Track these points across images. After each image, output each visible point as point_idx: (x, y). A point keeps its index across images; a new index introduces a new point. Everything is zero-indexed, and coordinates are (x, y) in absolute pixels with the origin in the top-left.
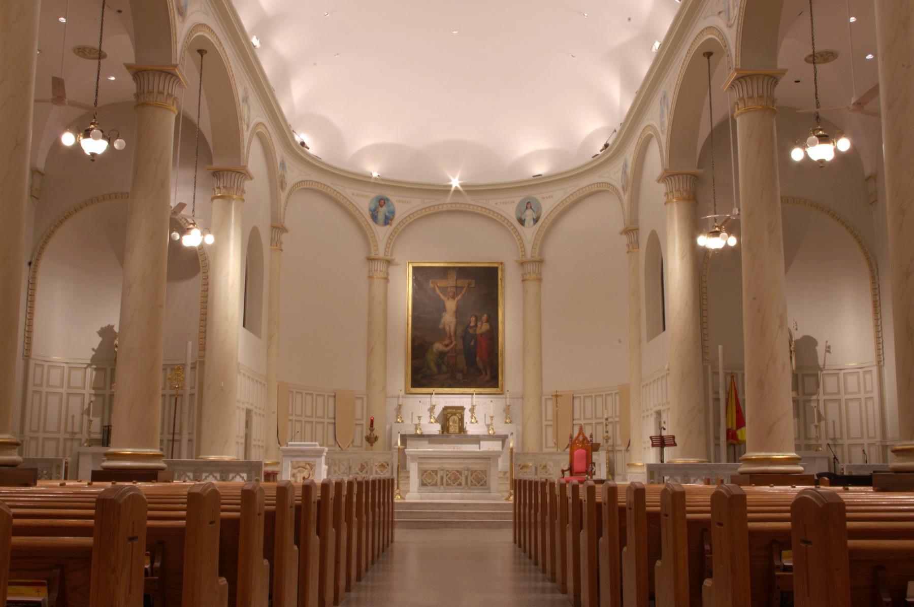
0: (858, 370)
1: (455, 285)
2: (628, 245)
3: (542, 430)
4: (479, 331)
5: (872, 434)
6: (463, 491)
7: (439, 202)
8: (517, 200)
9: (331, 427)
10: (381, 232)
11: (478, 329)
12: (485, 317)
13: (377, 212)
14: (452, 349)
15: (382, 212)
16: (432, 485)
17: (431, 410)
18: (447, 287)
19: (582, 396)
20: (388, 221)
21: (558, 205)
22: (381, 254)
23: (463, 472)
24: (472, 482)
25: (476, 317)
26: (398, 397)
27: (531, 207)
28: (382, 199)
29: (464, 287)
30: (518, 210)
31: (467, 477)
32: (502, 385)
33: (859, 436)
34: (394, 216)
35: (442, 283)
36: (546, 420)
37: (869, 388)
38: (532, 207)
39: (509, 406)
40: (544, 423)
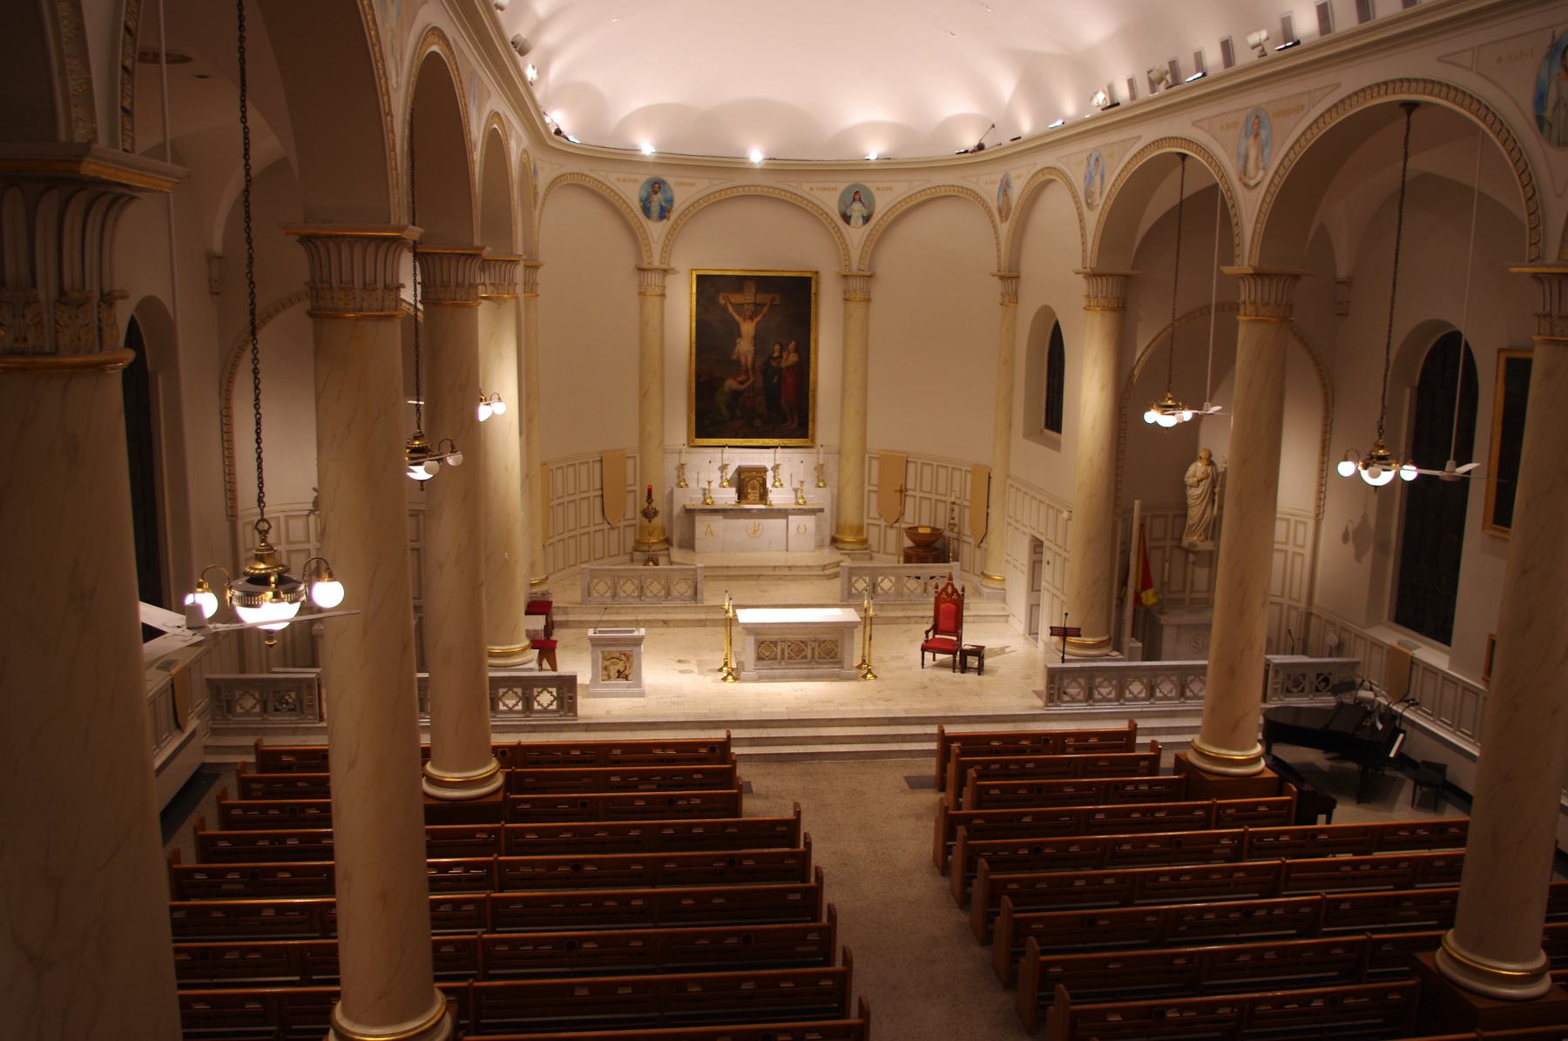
0: (1291, 517)
1: (753, 301)
2: (1002, 295)
3: (863, 497)
4: (784, 365)
5: (1295, 595)
6: (809, 666)
7: (729, 185)
8: (842, 187)
9: (598, 501)
10: (656, 230)
11: (784, 361)
12: (792, 345)
13: (650, 202)
14: (749, 386)
15: (657, 199)
16: (770, 659)
17: (723, 468)
18: (743, 304)
19: (920, 461)
20: (664, 213)
21: (899, 203)
22: (656, 263)
23: (809, 643)
24: (819, 654)
25: (781, 346)
26: (680, 452)
27: (860, 200)
28: (656, 183)
29: (766, 304)
30: (842, 201)
31: (813, 649)
32: (813, 435)
33: (1279, 594)
34: (672, 206)
35: (736, 298)
36: (870, 484)
37: (1300, 541)
38: (862, 199)
39: (822, 465)
40: (867, 488)
